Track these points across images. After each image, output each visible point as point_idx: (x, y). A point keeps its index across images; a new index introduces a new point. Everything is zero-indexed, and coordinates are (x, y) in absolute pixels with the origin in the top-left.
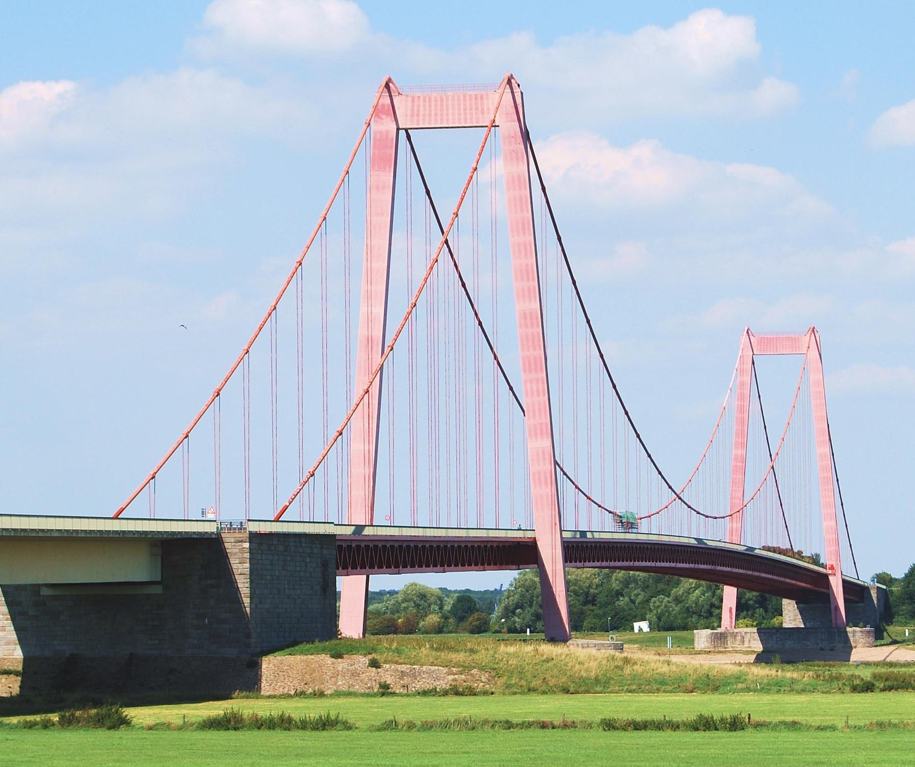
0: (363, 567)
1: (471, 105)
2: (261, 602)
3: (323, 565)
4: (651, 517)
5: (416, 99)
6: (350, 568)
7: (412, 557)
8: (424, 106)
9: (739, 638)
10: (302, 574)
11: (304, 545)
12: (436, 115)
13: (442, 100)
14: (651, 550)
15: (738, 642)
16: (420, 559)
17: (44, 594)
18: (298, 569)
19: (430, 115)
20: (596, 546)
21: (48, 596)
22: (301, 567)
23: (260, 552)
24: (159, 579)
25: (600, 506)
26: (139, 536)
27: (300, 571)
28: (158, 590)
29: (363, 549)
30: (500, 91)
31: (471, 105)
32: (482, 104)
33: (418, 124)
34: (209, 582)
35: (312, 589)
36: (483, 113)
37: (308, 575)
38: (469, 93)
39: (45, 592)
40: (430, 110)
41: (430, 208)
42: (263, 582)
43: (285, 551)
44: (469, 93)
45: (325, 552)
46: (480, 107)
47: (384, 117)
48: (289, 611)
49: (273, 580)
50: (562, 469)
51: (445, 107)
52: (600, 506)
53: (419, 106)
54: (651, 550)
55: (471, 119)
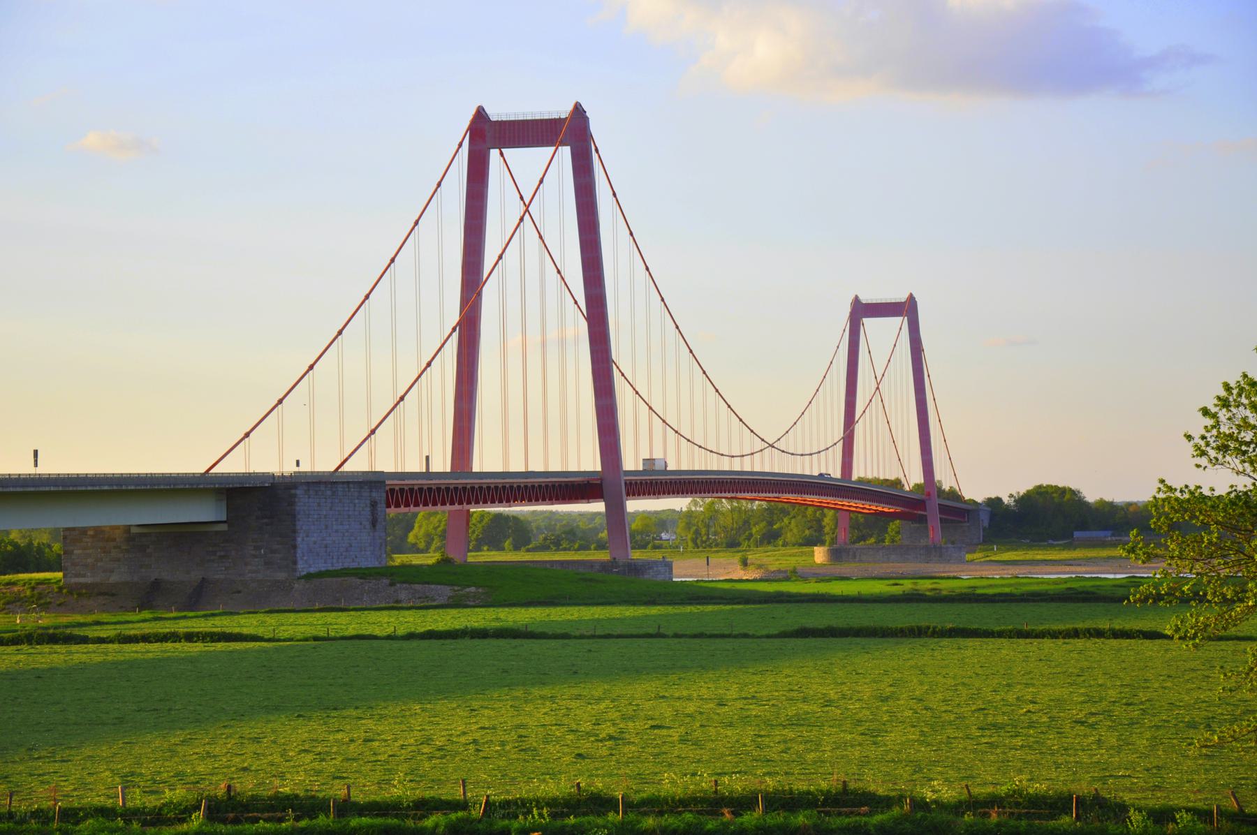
2: (307, 536)
3: (373, 506)
4: (755, 455)
6: (465, 504)
7: (550, 493)
10: (350, 513)
11: (352, 490)
14: (685, 484)
16: (646, 486)
17: (134, 532)
18: (347, 509)
20: (738, 482)
21: (137, 533)
22: (349, 507)
23: (307, 496)
24: (224, 518)
25: (689, 440)
26: (190, 487)
27: (349, 510)
28: (224, 527)
29: (460, 492)
30: (713, 696)
34: (265, 521)
35: (361, 524)
37: (356, 513)
39: (134, 530)
41: (460, 145)
42: (310, 519)
43: (333, 495)
45: (374, 494)
48: (337, 542)
49: (320, 518)
50: (618, 367)
52: (689, 440)
54: (685, 484)
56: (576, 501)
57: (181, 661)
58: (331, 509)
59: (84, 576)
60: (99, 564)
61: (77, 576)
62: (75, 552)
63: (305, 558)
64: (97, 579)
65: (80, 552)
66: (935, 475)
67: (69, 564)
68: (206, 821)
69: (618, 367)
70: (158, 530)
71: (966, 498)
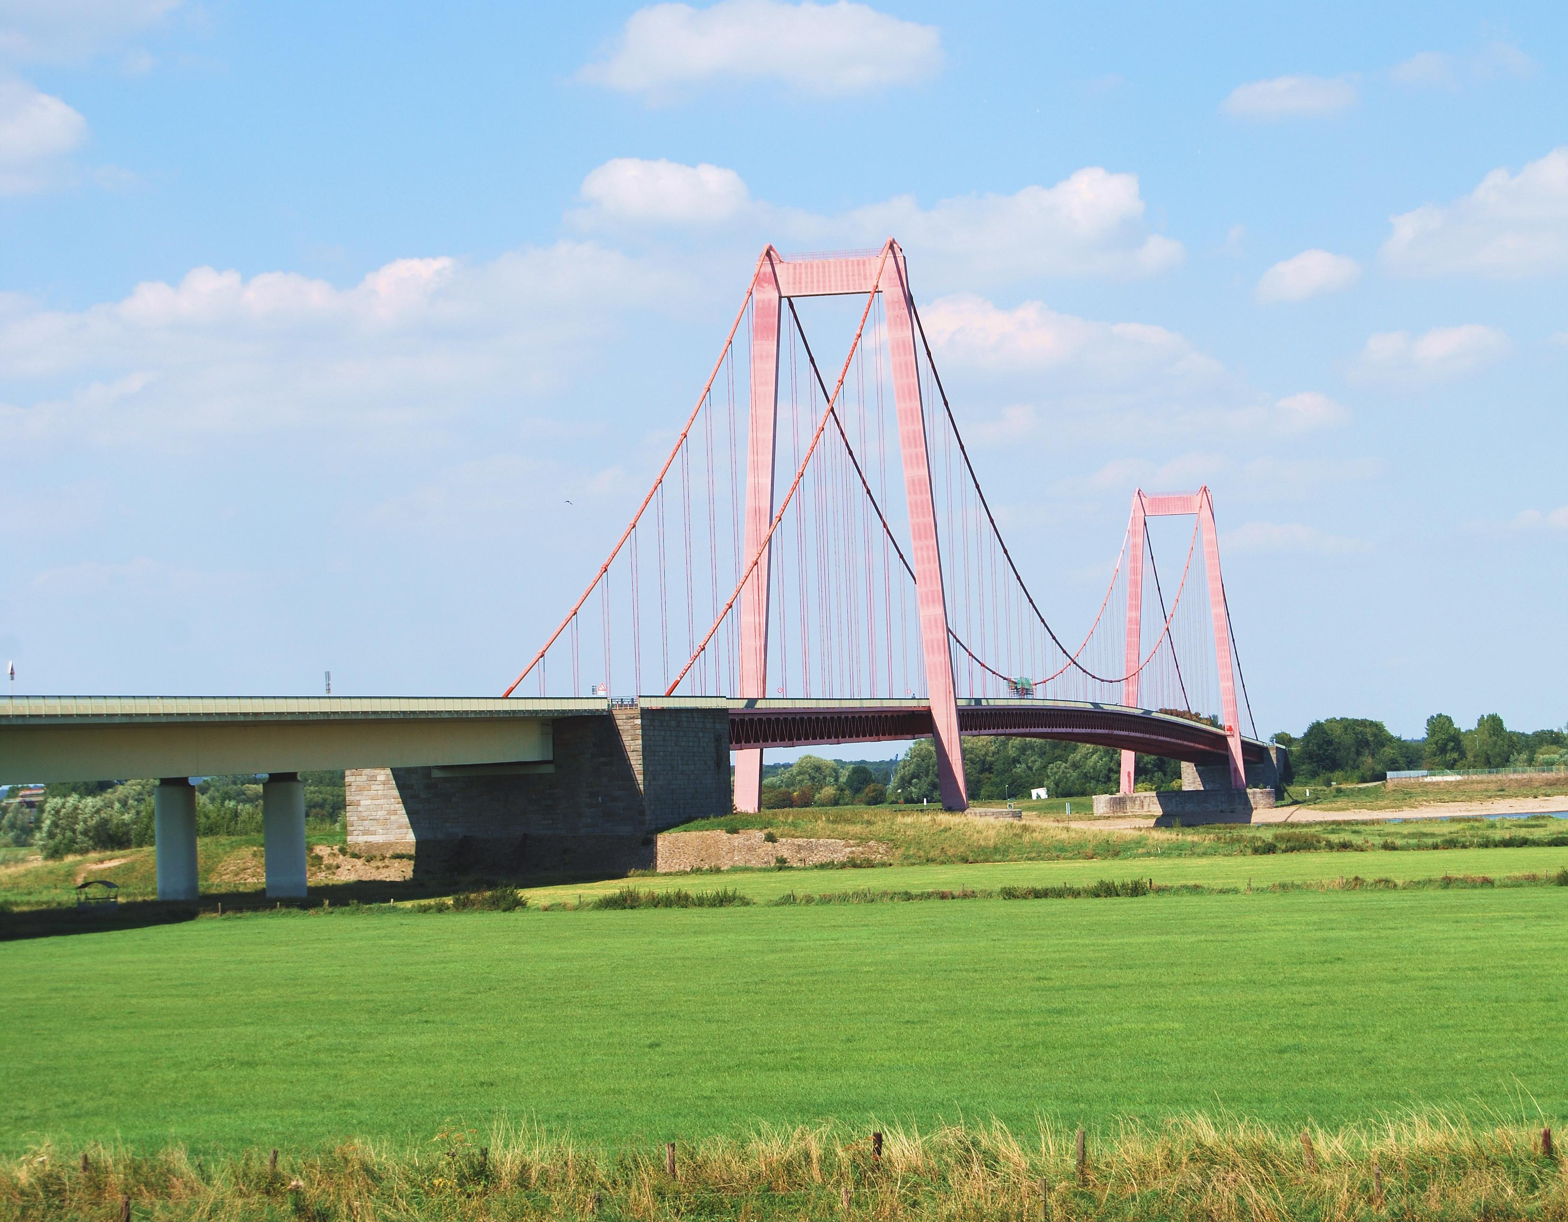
0: (757, 740)
1: (853, 270)
3: (717, 740)
5: (798, 267)
8: (806, 273)
9: (1138, 802)
10: (695, 749)
12: (818, 282)
13: (824, 267)
15: (1137, 807)
18: (691, 744)
19: (812, 282)
25: (994, 673)
28: (550, 769)
31: (853, 270)
32: (865, 270)
33: (801, 292)
36: (865, 279)
38: (851, 259)
39: (436, 774)
40: (812, 277)
44: (851, 259)
45: (718, 726)
46: (862, 272)
47: (766, 285)
50: (955, 637)
51: (827, 274)
53: (800, 273)
55: (854, 285)
56: (902, 736)
57: (932, 854)
58: (676, 745)
59: (374, 833)
60: (393, 818)
61: (366, 832)
62: (362, 803)
63: (652, 807)
64: (391, 838)
65: (369, 802)
66: (44, 940)
67: (356, 818)
68: (1204, 1203)
69: (955, 637)
70: (449, 774)
71: (1463, 730)
